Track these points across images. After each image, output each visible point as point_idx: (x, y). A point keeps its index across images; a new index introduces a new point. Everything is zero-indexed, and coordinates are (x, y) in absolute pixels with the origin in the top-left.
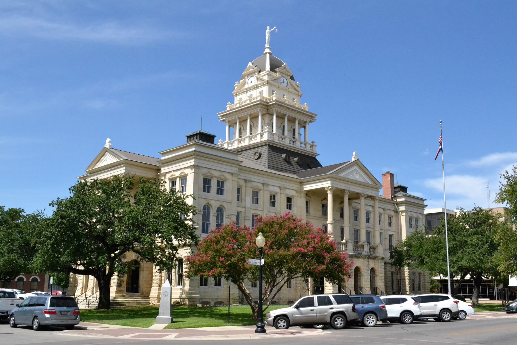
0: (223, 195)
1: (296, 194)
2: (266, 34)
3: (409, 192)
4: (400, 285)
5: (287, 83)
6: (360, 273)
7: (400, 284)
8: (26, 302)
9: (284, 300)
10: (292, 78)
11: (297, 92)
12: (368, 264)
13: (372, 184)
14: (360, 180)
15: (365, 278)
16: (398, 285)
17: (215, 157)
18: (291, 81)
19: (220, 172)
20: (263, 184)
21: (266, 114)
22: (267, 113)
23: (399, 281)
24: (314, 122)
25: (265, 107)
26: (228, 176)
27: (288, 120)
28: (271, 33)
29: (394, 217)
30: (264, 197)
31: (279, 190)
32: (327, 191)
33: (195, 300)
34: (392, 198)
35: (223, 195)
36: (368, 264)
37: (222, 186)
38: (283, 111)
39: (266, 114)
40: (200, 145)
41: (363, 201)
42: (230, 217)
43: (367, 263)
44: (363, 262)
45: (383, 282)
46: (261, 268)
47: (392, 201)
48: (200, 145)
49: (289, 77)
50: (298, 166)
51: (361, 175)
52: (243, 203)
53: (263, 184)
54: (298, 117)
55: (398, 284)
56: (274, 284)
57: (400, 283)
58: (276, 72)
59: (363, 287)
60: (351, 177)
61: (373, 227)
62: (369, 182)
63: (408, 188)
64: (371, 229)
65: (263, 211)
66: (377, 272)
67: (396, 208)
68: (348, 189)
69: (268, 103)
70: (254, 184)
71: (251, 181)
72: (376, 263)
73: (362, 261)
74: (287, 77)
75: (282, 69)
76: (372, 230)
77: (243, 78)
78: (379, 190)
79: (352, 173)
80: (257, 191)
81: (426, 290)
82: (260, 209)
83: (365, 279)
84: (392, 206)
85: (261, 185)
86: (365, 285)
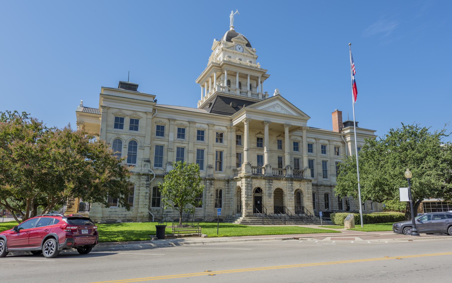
0: (123, 129)
1: (227, 129)
2: (230, 17)
3: (360, 126)
4: (348, 205)
5: (243, 50)
6: (302, 195)
7: (349, 204)
8: (139, 216)
9: (210, 218)
10: (248, 45)
11: (253, 56)
12: (292, 186)
13: (298, 115)
14: (283, 113)
15: (287, 198)
16: (346, 205)
17: (133, 100)
18: (247, 48)
19: (118, 110)
20: (189, 122)
21: (222, 74)
22: (221, 73)
23: (347, 201)
24: (268, 77)
25: (219, 68)
26: (141, 114)
27: (239, 77)
28: (235, 16)
29: (341, 147)
30: (317, 148)
31: (208, 127)
32: (244, 123)
33: (96, 218)
34: (340, 132)
35: (123, 129)
36: (292, 186)
37: (325, 148)
38: (234, 69)
39: (222, 74)
40: (110, 90)
41: (304, 133)
42: (143, 148)
43: (291, 185)
44: (285, 184)
45: (311, 202)
46: (77, 189)
47: (340, 134)
48: (110, 90)
49: (245, 45)
50: (233, 109)
51: (283, 108)
52: (166, 138)
53: (189, 122)
54: (249, 73)
55: (347, 204)
56: (4, 205)
57: (348, 203)
58: (232, 42)
59: (286, 206)
60: (272, 110)
61: (316, 156)
62: (294, 114)
63: (358, 122)
64: (223, 148)
65: (189, 144)
66: (304, 192)
67: (343, 140)
68: (288, 123)
69: (220, 64)
70: (159, 119)
71: (175, 120)
72: (303, 185)
73: (284, 183)
74: (242, 44)
75: (238, 39)
76: (315, 158)
77: (213, 51)
78: (307, 121)
79: (274, 106)
80: (281, 140)
81: (378, 209)
82: (186, 142)
83: (287, 199)
84: (338, 138)
85: (187, 123)
86: (266, 204)
